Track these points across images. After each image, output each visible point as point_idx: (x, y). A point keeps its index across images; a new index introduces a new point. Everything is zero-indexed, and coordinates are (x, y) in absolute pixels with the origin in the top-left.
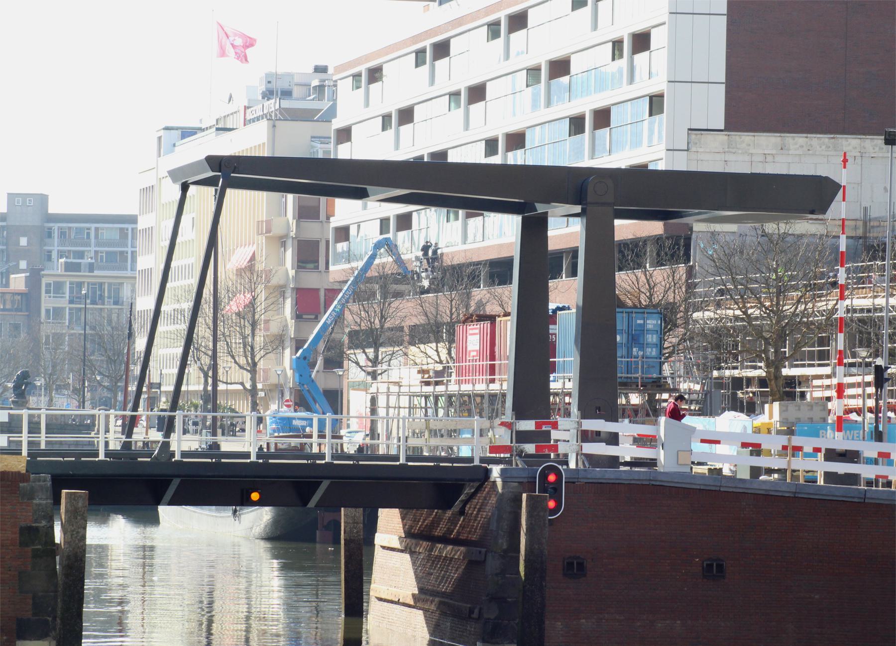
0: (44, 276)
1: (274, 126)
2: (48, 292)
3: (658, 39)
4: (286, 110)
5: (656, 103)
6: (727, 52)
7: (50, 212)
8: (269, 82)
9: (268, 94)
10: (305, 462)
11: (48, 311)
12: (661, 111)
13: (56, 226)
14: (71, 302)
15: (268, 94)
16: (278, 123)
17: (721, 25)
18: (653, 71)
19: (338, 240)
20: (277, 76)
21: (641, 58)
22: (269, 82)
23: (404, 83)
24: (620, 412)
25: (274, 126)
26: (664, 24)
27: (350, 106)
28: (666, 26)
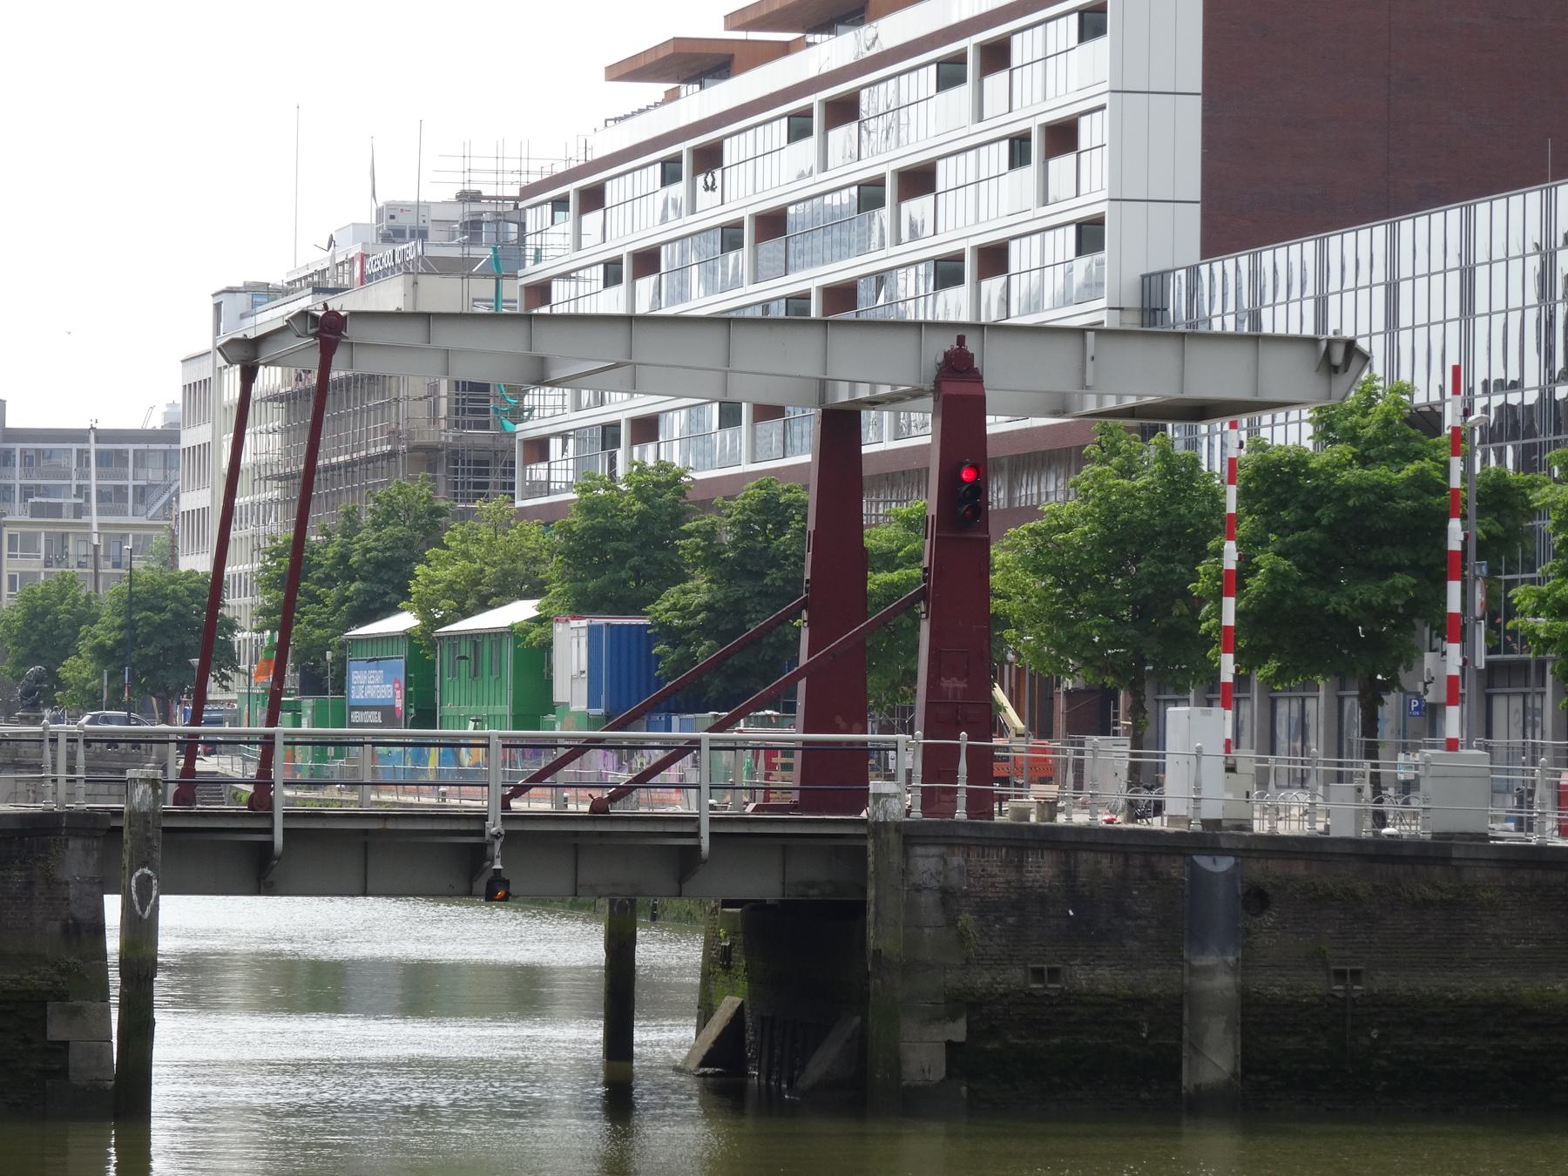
0: (5, 524)
1: (415, 283)
2: (12, 546)
3: (1089, 131)
4: (434, 259)
5: (1089, 235)
6: (1203, 155)
7: (9, 425)
8: (392, 217)
9: (393, 235)
10: (113, 944)
11: (12, 578)
12: (1099, 247)
13: (18, 447)
14: (48, 563)
15: (393, 235)
16: (422, 279)
17: (1192, 112)
18: (1085, 181)
19: (529, 460)
20: (403, 208)
21: (1062, 165)
22: (392, 217)
23: (640, 211)
24: (830, 820)
25: (415, 283)
26: (1102, 108)
27: (553, 242)
28: (1106, 112)
